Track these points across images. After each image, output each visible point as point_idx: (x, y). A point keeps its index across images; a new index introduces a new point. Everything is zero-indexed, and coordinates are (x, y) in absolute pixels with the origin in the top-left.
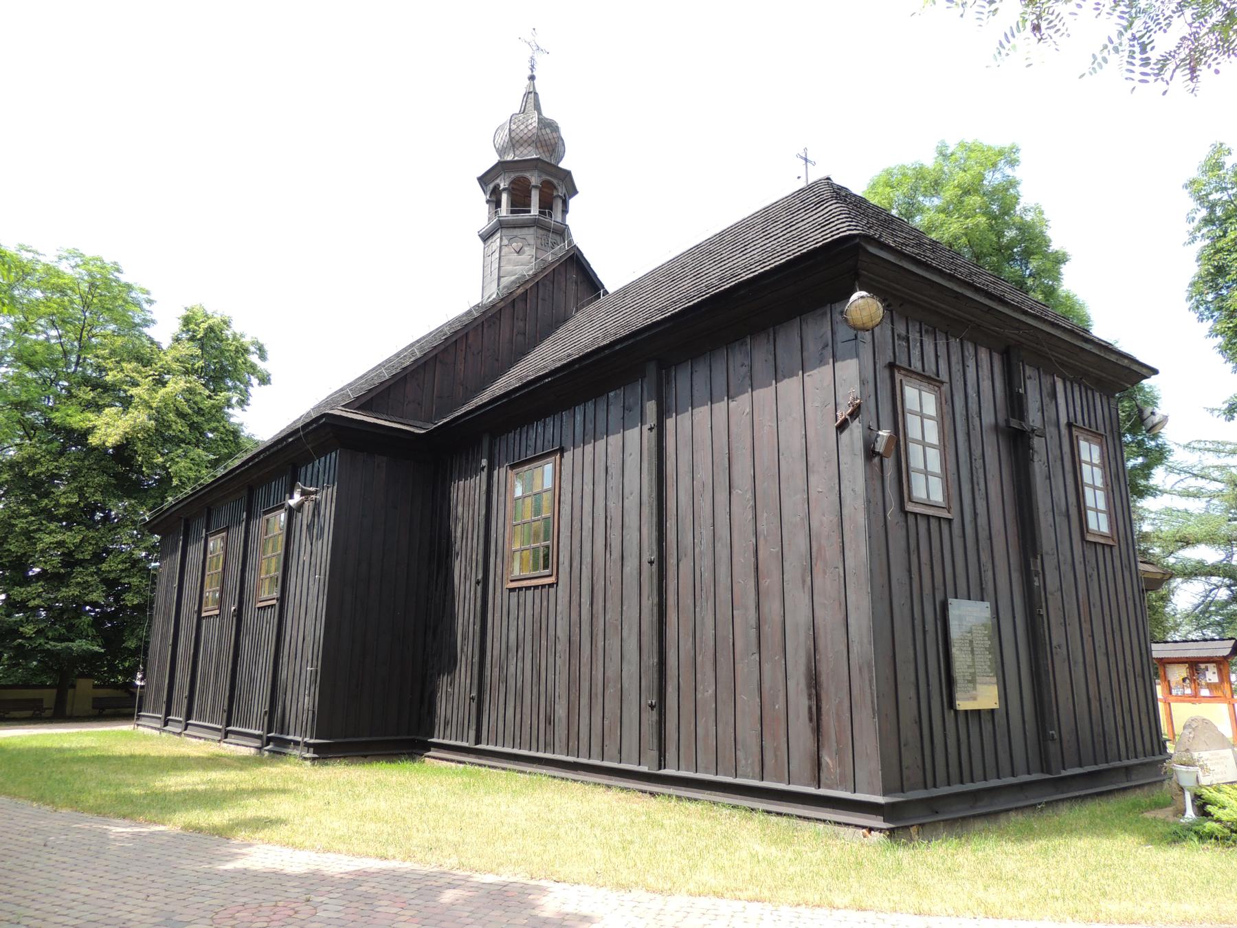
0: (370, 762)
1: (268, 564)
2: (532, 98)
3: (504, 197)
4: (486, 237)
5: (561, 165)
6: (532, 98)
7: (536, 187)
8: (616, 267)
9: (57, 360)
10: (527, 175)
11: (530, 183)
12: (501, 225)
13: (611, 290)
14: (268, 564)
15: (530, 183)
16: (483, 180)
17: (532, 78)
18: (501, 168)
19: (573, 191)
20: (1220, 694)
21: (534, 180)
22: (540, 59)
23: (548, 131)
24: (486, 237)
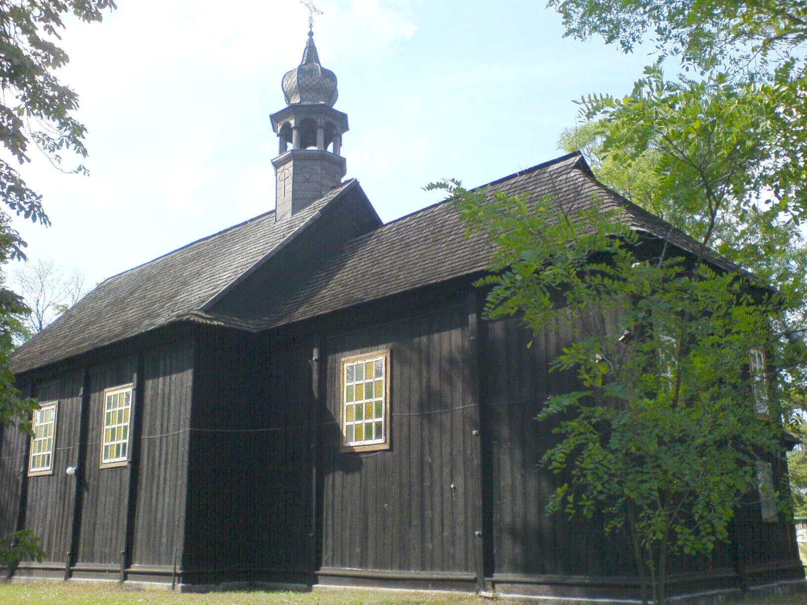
0: (224, 590)
1: (161, 386)
2: (311, 52)
3: (295, 133)
4: (277, 165)
5: (336, 107)
6: (311, 52)
7: (322, 127)
8: (392, 203)
9: (737, 231)
10: (314, 116)
11: (311, 119)
12: (294, 156)
13: (384, 222)
14: (161, 386)
15: (311, 119)
16: (275, 118)
17: (311, 34)
18: (292, 110)
19: (346, 128)
20: (695, 408)
21: (320, 121)
22: (315, 16)
23: (328, 80)
24: (277, 165)
